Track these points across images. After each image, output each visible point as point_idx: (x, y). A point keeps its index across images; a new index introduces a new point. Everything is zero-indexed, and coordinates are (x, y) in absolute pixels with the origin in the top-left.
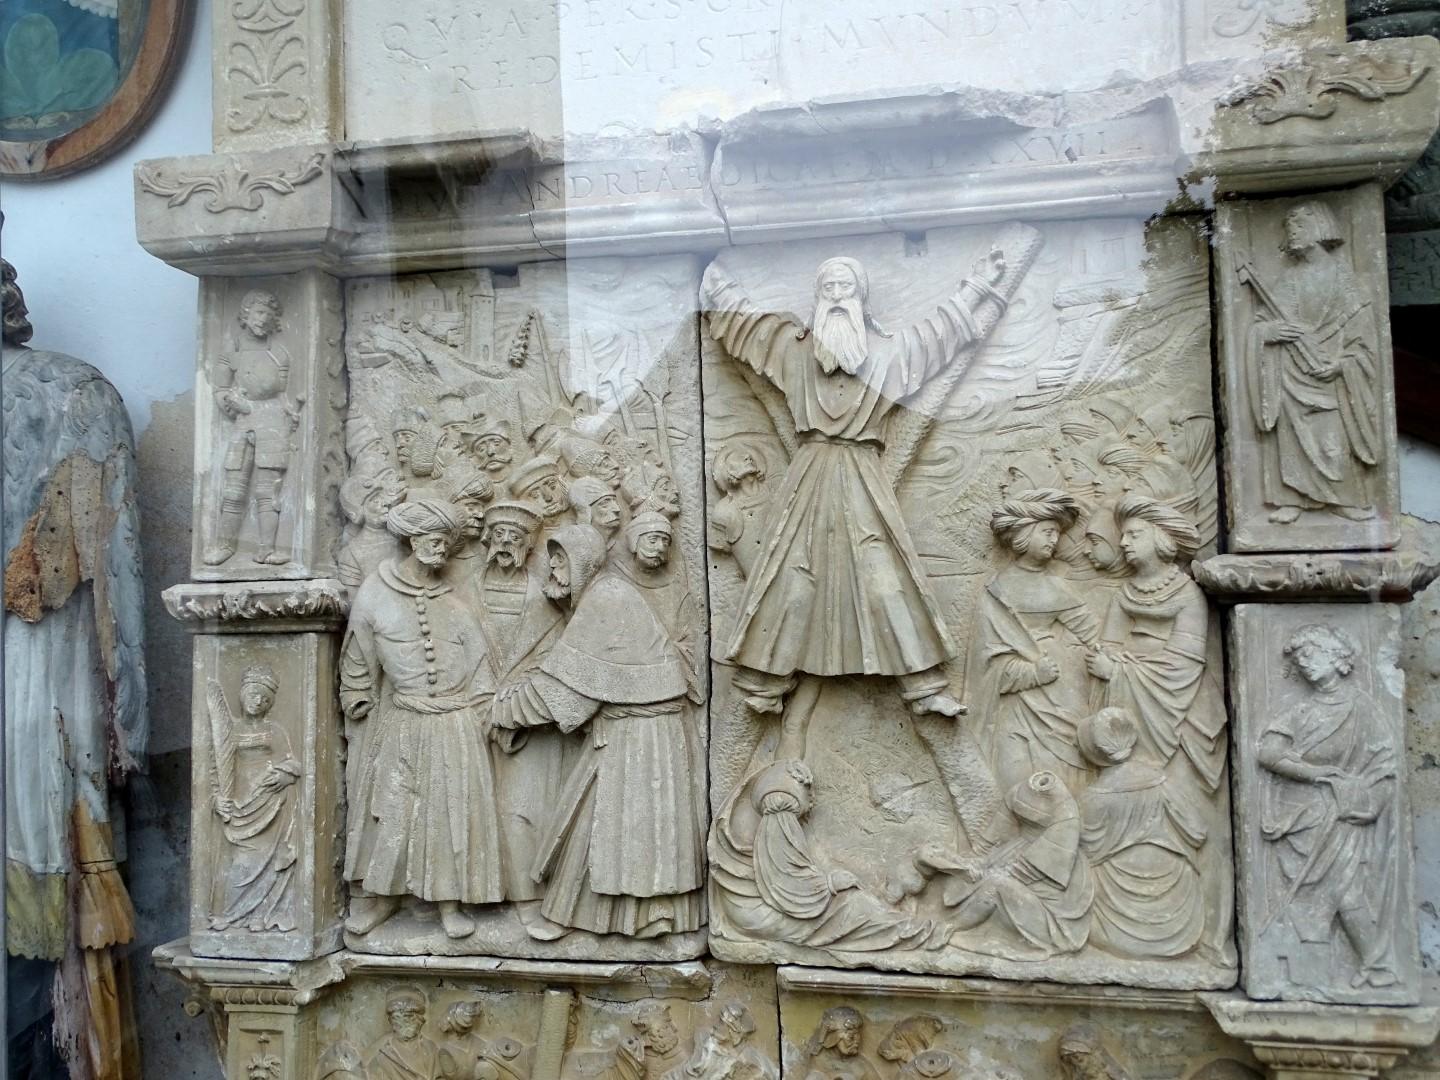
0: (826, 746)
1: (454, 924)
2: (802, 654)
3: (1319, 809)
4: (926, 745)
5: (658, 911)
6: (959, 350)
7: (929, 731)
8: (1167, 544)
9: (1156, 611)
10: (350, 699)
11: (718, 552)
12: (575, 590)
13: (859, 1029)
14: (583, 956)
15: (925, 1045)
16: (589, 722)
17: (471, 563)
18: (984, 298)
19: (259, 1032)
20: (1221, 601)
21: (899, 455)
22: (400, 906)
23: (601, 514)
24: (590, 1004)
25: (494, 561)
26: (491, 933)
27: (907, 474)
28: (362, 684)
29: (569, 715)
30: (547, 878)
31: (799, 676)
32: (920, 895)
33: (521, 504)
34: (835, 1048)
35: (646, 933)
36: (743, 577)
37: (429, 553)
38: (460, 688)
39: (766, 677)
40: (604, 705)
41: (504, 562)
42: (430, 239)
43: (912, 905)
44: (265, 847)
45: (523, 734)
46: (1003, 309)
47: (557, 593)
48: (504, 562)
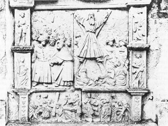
0: (90, 64)
1: (45, 85)
2: (86, 56)
3: (138, 70)
4: (98, 65)
5: (69, 83)
6: (103, 23)
7: (99, 64)
8: (124, 44)
9: (123, 51)
10: (33, 60)
11: (75, 44)
12: (61, 48)
13: (91, 95)
14: (61, 88)
15: (97, 96)
16: (62, 63)
17: (48, 45)
18: (106, 17)
19: (23, 98)
20: (132, 94)
21: (97, 34)
22: (39, 83)
23: (161, 16)
24: (61, 93)
25: (51, 45)
26: (49, 86)
27: (97, 36)
28: (34, 58)
29: (60, 62)
30: (57, 79)
31: (85, 58)
32: (89, 98)
33: (53, 38)
34: (88, 97)
35: (68, 85)
36: (78, 47)
37: (43, 43)
38: (47, 59)
39: (82, 58)
40: (64, 61)
41: (52, 45)
42: (42, 7)
43: (88, 98)
44: (24, 77)
45: (54, 64)
46: (108, 18)
47: (59, 48)
48: (52, 45)
